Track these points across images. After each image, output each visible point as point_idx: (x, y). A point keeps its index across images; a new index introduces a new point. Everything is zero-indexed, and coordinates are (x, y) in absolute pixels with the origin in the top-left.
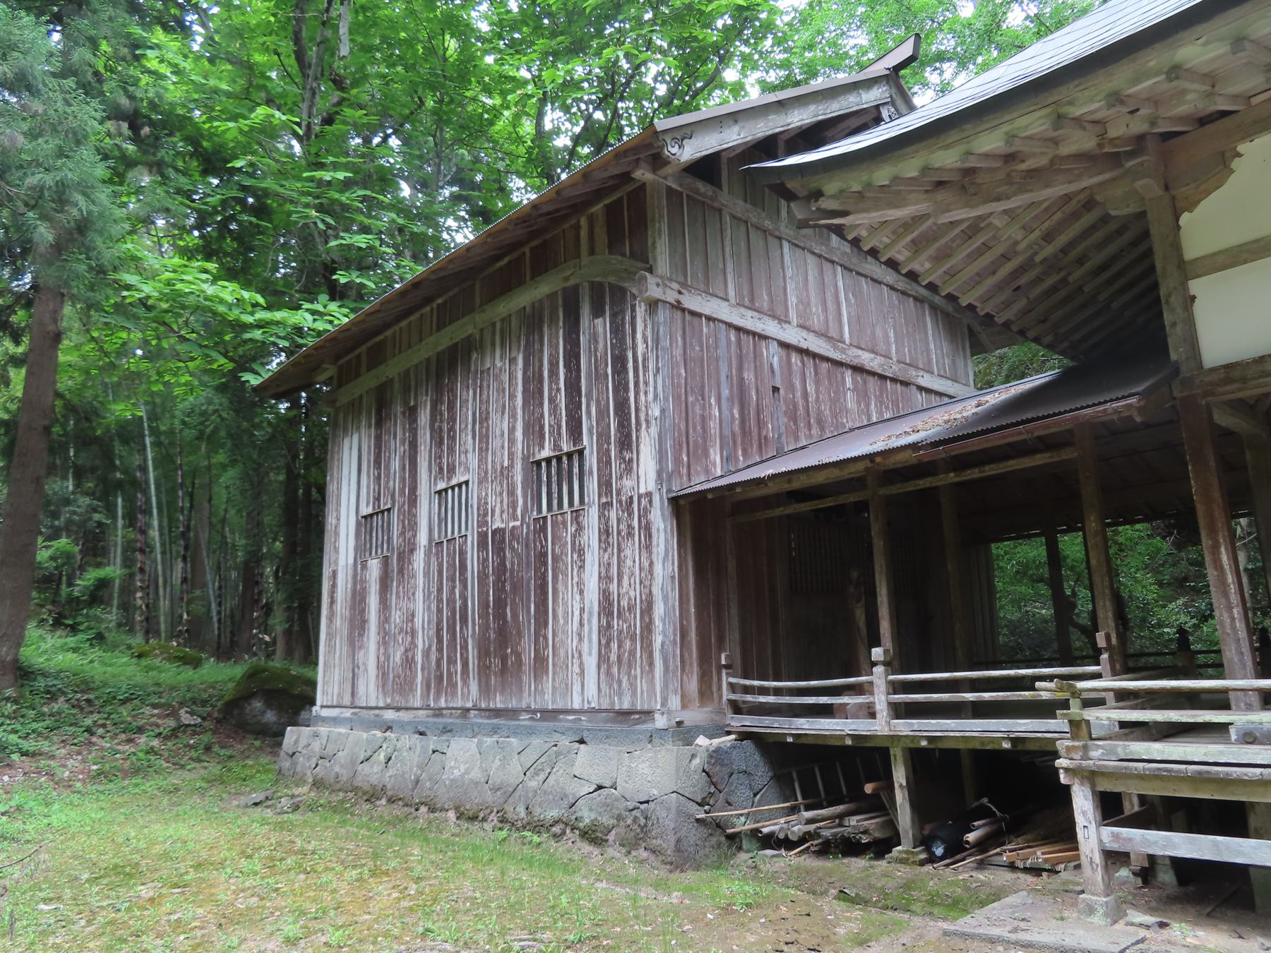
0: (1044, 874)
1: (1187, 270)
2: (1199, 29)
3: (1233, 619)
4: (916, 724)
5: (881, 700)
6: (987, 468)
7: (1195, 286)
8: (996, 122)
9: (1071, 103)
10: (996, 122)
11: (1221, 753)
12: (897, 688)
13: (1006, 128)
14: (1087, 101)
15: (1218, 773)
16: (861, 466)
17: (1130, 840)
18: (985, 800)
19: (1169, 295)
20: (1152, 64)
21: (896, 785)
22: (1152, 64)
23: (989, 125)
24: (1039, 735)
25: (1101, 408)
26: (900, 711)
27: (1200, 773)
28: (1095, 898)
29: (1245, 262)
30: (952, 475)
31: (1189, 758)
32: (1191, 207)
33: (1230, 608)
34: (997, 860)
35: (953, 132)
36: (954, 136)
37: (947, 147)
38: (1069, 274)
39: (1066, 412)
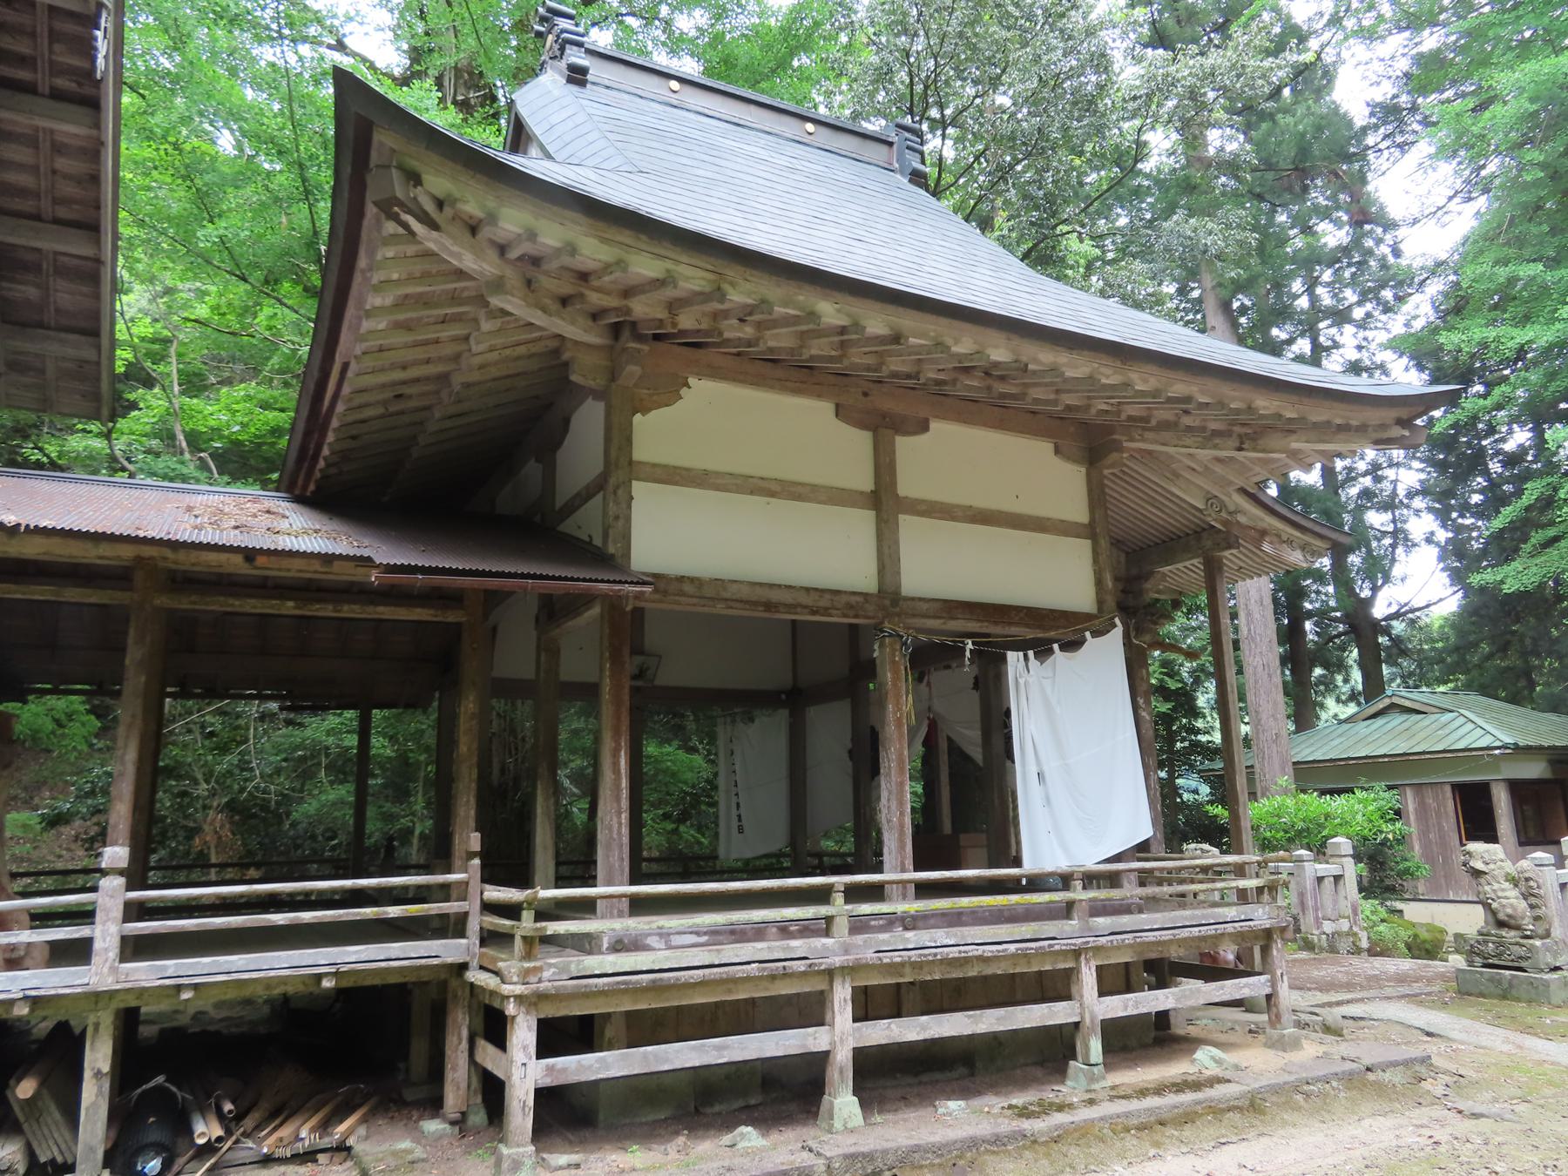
0: (320, 1157)
1: (635, 470)
2: (839, 296)
3: (620, 824)
4: (171, 966)
5: (106, 933)
6: (346, 608)
7: (638, 487)
8: (663, 252)
9: (732, 284)
10: (663, 252)
11: (667, 958)
12: (136, 911)
13: (669, 265)
14: (742, 291)
15: (637, 982)
16: (127, 552)
17: (564, 1070)
18: (160, 1079)
19: (618, 487)
20: (801, 298)
21: (88, 1074)
22: (801, 298)
23: (656, 251)
24: (423, 961)
25: (617, 587)
26: (134, 948)
27: (654, 981)
28: (521, 1150)
29: (676, 484)
30: (291, 604)
31: (639, 968)
32: (645, 410)
33: (619, 813)
34: (240, 1155)
35: (627, 232)
36: (626, 236)
37: (604, 241)
38: (1279, 539)
39: (578, 580)
